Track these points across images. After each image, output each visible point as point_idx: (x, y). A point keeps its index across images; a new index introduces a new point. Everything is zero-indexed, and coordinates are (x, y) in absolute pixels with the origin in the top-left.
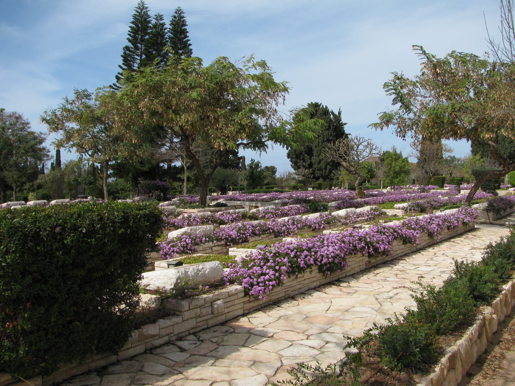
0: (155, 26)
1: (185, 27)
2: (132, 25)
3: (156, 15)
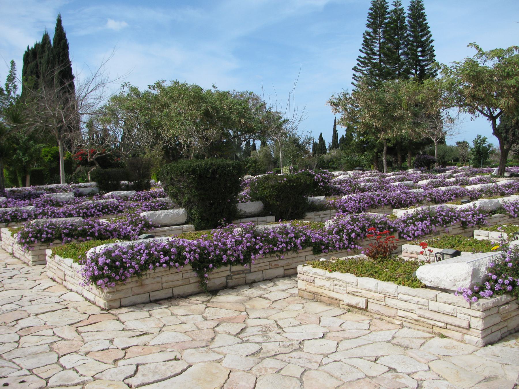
0: (395, 11)
1: (423, 11)
2: (371, 12)
3: (394, 2)
